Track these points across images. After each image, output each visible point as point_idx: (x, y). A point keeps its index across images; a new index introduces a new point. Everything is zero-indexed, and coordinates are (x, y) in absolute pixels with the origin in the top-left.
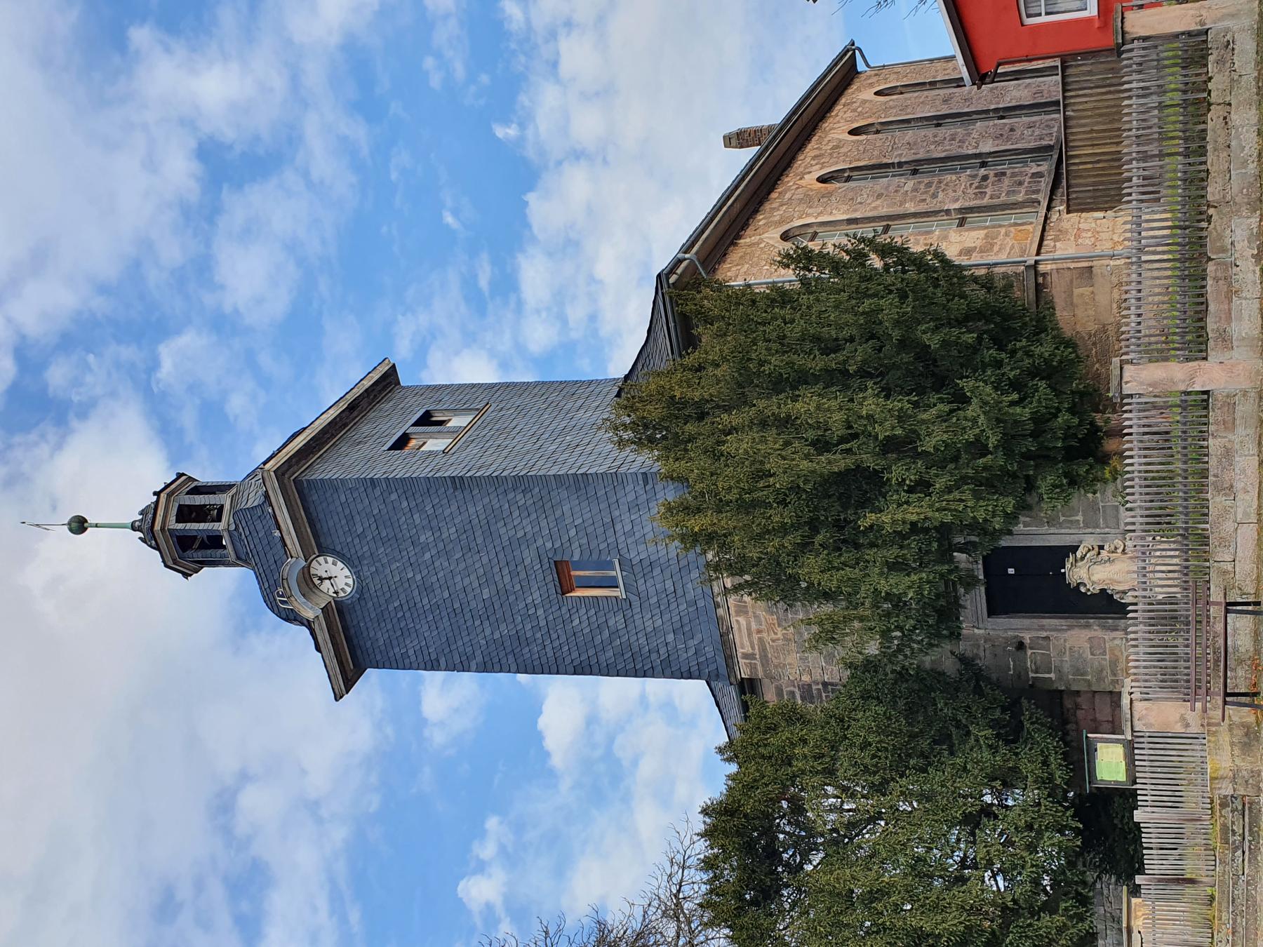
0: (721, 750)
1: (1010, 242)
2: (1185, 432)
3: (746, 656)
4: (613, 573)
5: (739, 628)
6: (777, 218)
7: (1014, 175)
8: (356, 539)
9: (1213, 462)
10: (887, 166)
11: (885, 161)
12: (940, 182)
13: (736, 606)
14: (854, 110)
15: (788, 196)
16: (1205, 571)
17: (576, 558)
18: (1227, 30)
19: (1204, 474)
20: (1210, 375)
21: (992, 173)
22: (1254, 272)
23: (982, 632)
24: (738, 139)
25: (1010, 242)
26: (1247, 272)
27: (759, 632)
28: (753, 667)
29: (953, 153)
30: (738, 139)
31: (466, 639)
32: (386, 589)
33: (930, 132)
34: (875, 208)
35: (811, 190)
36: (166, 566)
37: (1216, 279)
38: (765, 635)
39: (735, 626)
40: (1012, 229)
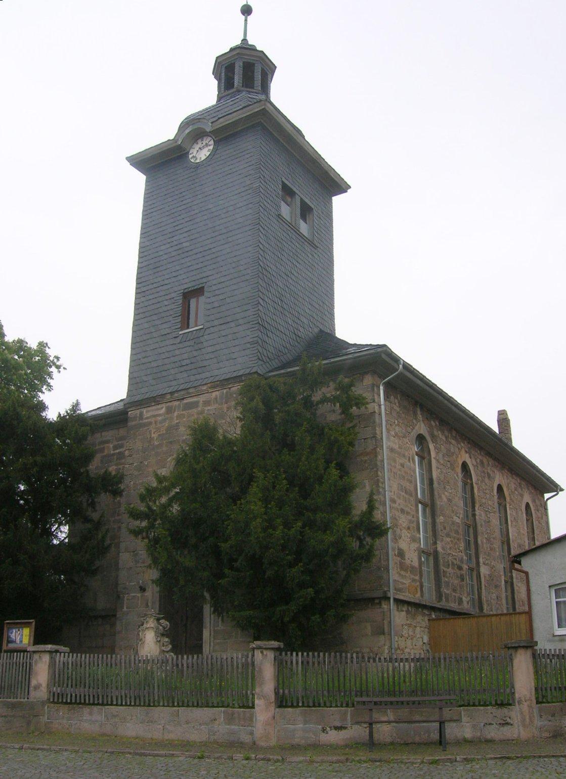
2: (117, 688)
3: (141, 414)
5: (158, 409)
8: (241, 179)
10: (473, 507)
13: (172, 406)
14: (516, 489)
20: (263, 711)
24: (503, 419)
27: (156, 422)
28: (135, 418)
29: (480, 549)
30: (503, 419)
35: (457, 457)
38: (154, 425)
39: (160, 406)
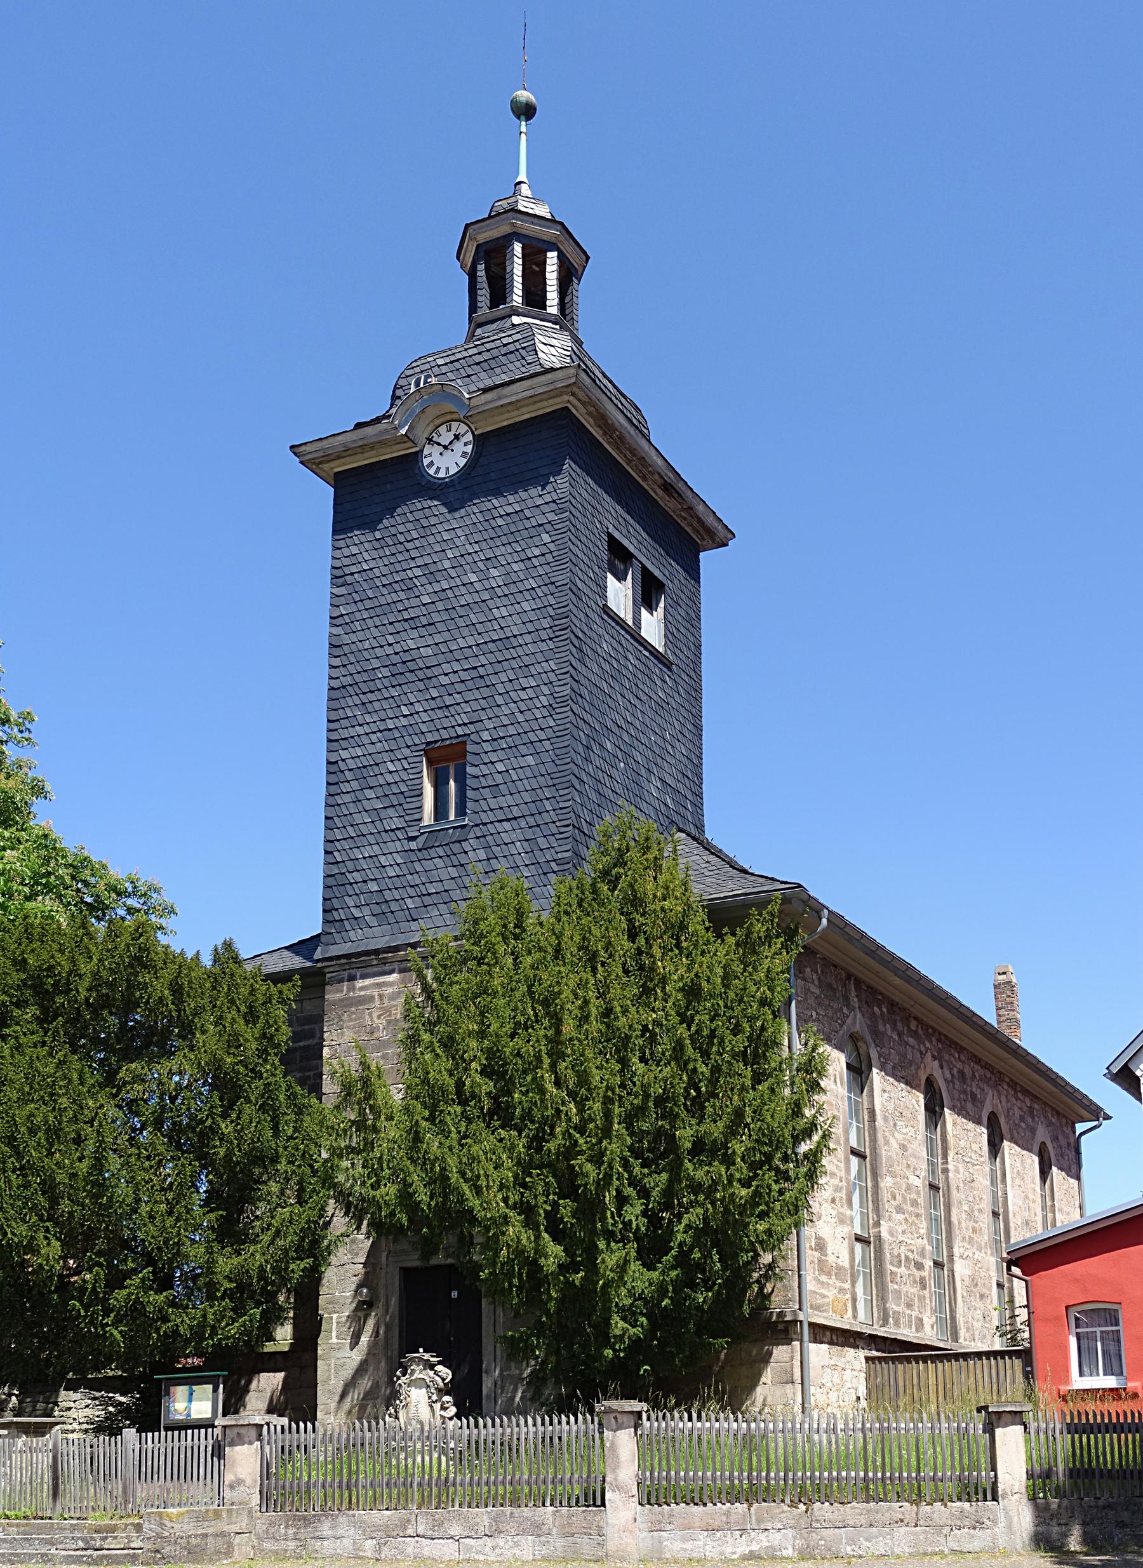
0: (228, 945)
1: (831, 1293)
4: (452, 817)
6: (881, 1028)
7: (922, 1299)
9: (526, 1512)
11: (951, 1154)
12: (917, 1216)
14: (1022, 1119)
15: (911, 1041)
16: (402, 1503)
17: (469, 770)
18: (995, 1522)
19: (515, 1502)
20: (622, 1509)
21: (925, 1274)
22: (734, 1553)
23: (384, 1258)
25: (831, 1293)
26: (736, 1546)
31: (370, 622)
32: (433, 520)
33: (986, 1206)
34: (887, 1142)
36: (467, 226)
37: (727, 1514)
40: (848, 1296)
